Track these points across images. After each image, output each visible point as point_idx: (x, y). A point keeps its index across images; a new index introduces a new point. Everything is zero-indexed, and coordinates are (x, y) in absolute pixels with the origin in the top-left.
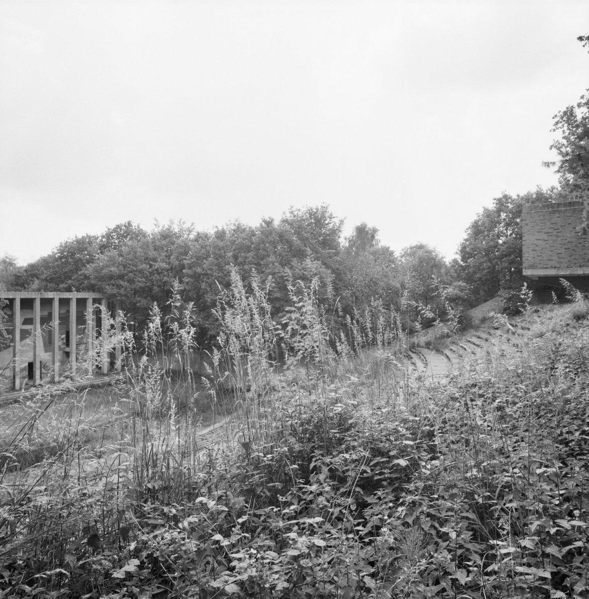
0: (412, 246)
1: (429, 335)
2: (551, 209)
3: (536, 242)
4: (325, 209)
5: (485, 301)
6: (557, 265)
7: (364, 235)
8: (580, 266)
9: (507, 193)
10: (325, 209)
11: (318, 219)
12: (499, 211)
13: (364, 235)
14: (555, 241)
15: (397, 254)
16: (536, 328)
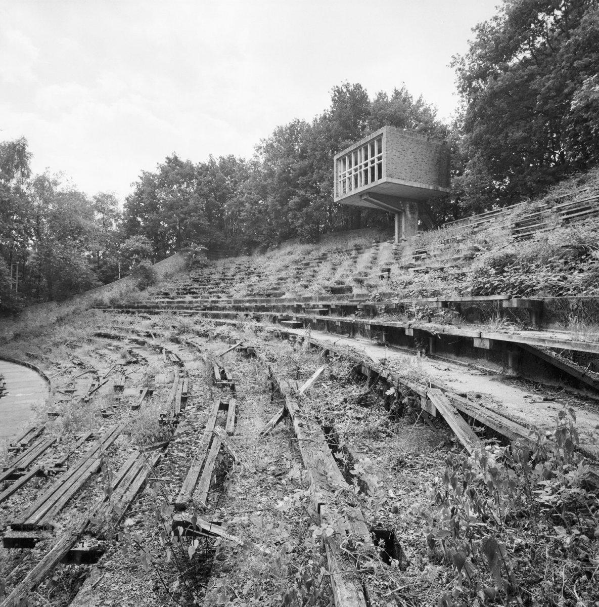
1: (114, 290)
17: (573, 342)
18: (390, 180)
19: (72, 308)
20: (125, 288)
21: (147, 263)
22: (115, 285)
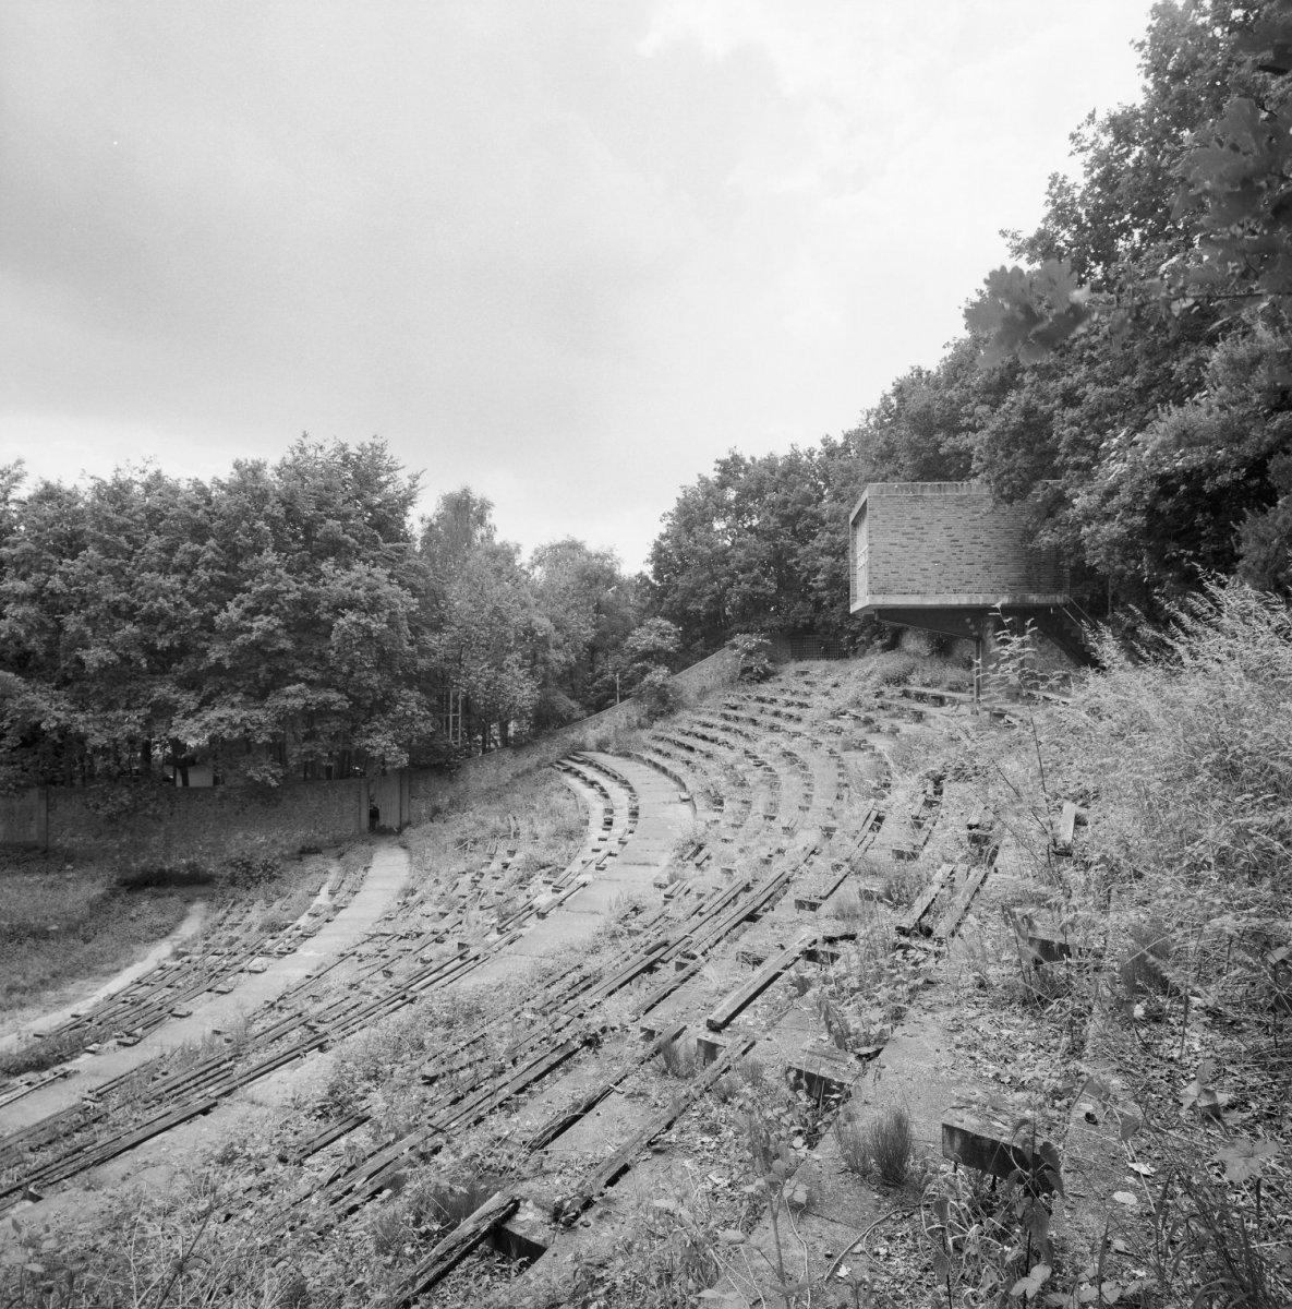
0: (554, 543)
1: (604, 726)
2: (911, 494)
3: (889, 548)
4: (377, 451)
5: (704, 656)
6: (922, 589)
7: (463, 512)
8: (955, 592)
9: (738, 452)
10: (377, 451)
11: (365, 473)
12: (723, 485)
13: (463, 512)
14: (918, 548)
15: (524, 559)
16: (820, 704)
17: (256, 1029)
18: (880, 600)
19: (536, 758)
20: (624, 720)
21: (659, 675)
22: (606, 715)
